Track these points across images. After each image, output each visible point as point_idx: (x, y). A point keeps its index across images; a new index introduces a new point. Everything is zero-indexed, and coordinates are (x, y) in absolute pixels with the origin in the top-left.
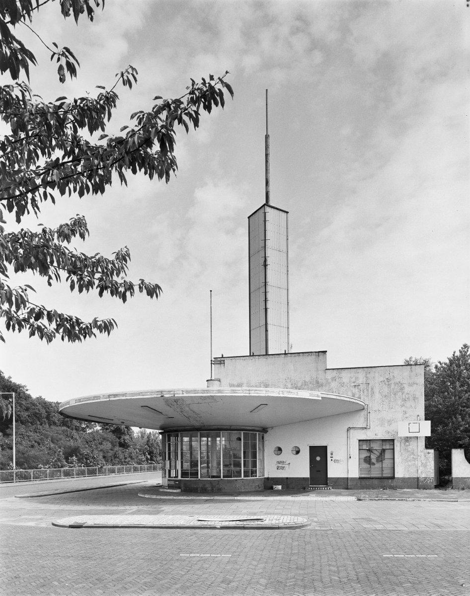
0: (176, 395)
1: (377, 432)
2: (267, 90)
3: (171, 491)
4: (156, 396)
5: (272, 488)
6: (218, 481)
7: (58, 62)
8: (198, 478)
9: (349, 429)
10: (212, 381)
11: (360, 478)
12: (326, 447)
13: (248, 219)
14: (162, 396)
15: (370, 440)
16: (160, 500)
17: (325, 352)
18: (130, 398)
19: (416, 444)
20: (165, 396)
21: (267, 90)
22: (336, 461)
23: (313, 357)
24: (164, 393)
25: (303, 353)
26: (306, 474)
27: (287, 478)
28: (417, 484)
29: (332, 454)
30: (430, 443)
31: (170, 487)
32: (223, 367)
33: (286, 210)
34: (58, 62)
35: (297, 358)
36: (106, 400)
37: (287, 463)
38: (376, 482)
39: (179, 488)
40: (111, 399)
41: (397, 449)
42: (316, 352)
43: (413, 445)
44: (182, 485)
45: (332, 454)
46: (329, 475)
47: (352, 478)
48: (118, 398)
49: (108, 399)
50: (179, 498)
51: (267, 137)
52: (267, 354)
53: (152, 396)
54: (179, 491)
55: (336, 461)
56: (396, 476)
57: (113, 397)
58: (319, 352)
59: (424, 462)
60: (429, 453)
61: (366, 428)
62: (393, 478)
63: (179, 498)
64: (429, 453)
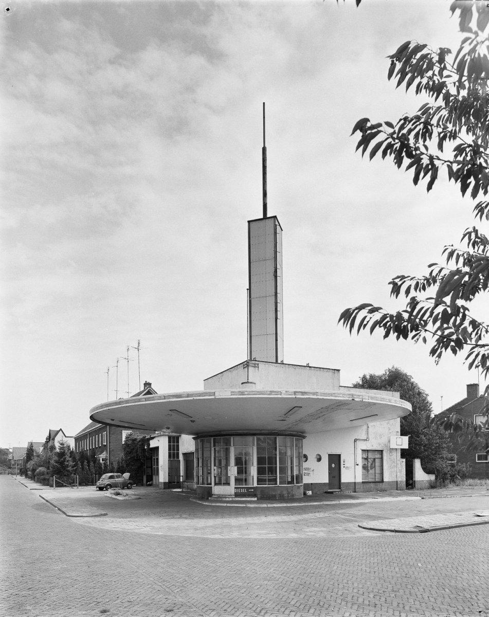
0: (364, 400)
1: (373, 445)
2: (264, 103)
3: (239, 499)
4: (348, 399)
5: (207, 494)
6: (292, 487)
7: (452, 76)
8: (277, 484)
9: (355, 441)
10: (248, 384)
11: (363, 482)
12: (339, 455)
13: (247, 224)
14: (353, 400)
15: (368, 450)
16: (293, 508)
17: (338, 370)
18: (322, 397)
19: (395, 454)
20: (355, 399)
21: (264, 103)
22: (347, 468)
23: (330, 373)
24: (355, 397)
25: (289, 365)
26: (325, 479)
27: (312, 484)
28: (396, 486)
29: (344, 462)
30: (404, 453)
31: (237, 495)
32: (257, 370)
33: (282, 228)
34: (452, 76)
35: (318, 372)
36: (290, 396)
37: (312, 469)
38: (372, 485)
39: (255, 496)
40: (298, 396)
41: (385, 458)
42: (332, 369)
43: (394, 454)
44: (258, 493)
45: (344, 462)
46: (343, 480)
47: (358, 483)
48: (308, 397)
49: (294, 396)
50: (293, 505)
51: (264, 149)
52: (277, 362)
53: (344, 399)
54: (256, 499)
55: (347, 468)
56: (384, 481)
57: (301, 394)
58: (335, 370)
59: (400, 468)
60: (403, 462)
61: (366, 440)
62: (382, 481)
63: (293, 505)
64: (403, 462)
